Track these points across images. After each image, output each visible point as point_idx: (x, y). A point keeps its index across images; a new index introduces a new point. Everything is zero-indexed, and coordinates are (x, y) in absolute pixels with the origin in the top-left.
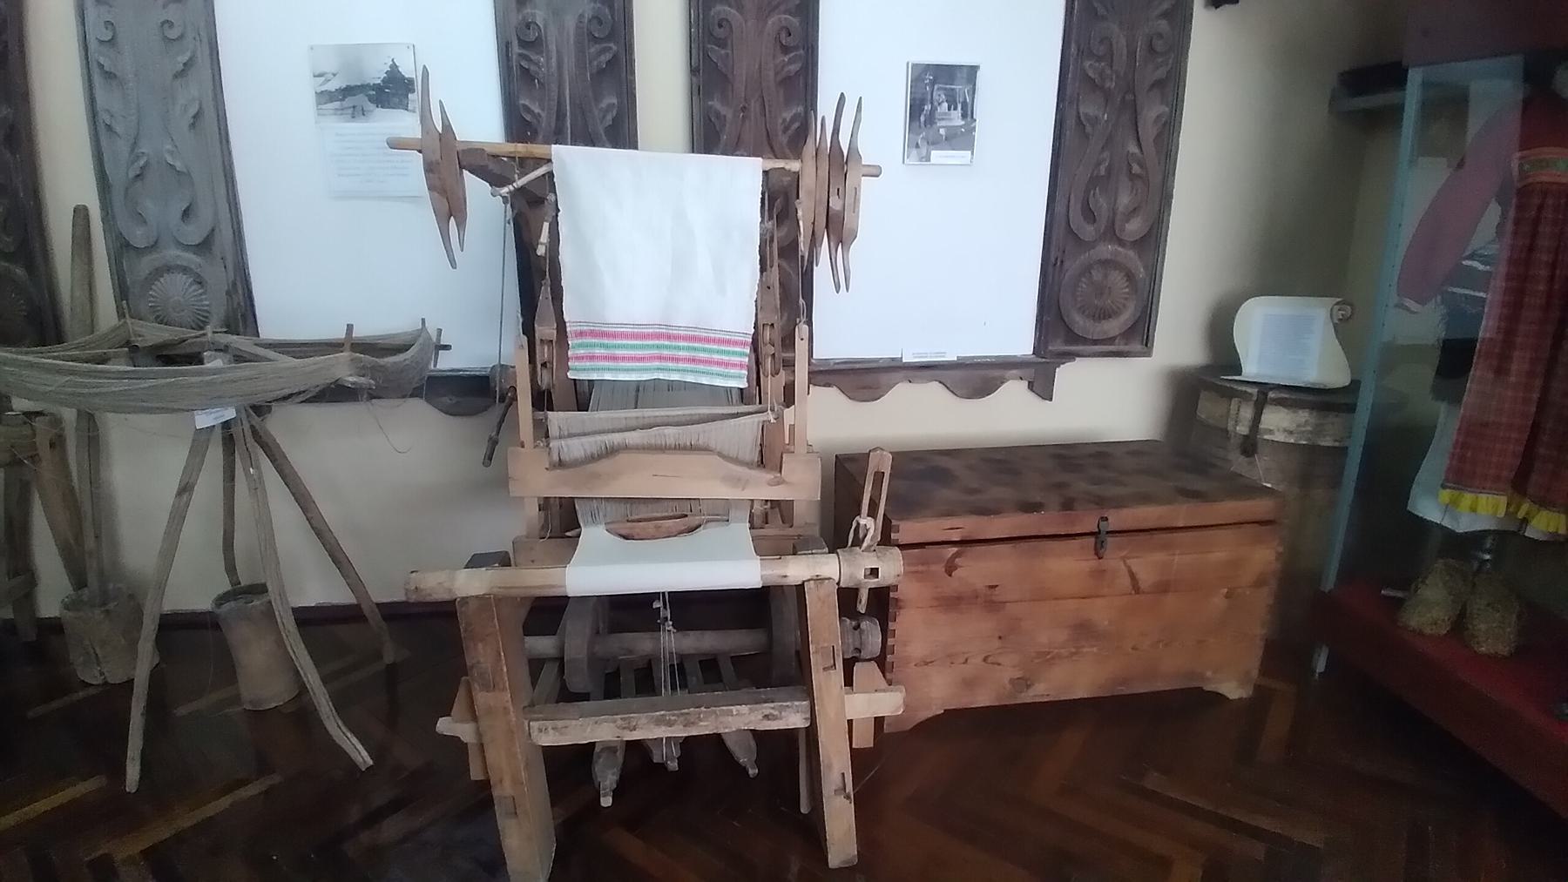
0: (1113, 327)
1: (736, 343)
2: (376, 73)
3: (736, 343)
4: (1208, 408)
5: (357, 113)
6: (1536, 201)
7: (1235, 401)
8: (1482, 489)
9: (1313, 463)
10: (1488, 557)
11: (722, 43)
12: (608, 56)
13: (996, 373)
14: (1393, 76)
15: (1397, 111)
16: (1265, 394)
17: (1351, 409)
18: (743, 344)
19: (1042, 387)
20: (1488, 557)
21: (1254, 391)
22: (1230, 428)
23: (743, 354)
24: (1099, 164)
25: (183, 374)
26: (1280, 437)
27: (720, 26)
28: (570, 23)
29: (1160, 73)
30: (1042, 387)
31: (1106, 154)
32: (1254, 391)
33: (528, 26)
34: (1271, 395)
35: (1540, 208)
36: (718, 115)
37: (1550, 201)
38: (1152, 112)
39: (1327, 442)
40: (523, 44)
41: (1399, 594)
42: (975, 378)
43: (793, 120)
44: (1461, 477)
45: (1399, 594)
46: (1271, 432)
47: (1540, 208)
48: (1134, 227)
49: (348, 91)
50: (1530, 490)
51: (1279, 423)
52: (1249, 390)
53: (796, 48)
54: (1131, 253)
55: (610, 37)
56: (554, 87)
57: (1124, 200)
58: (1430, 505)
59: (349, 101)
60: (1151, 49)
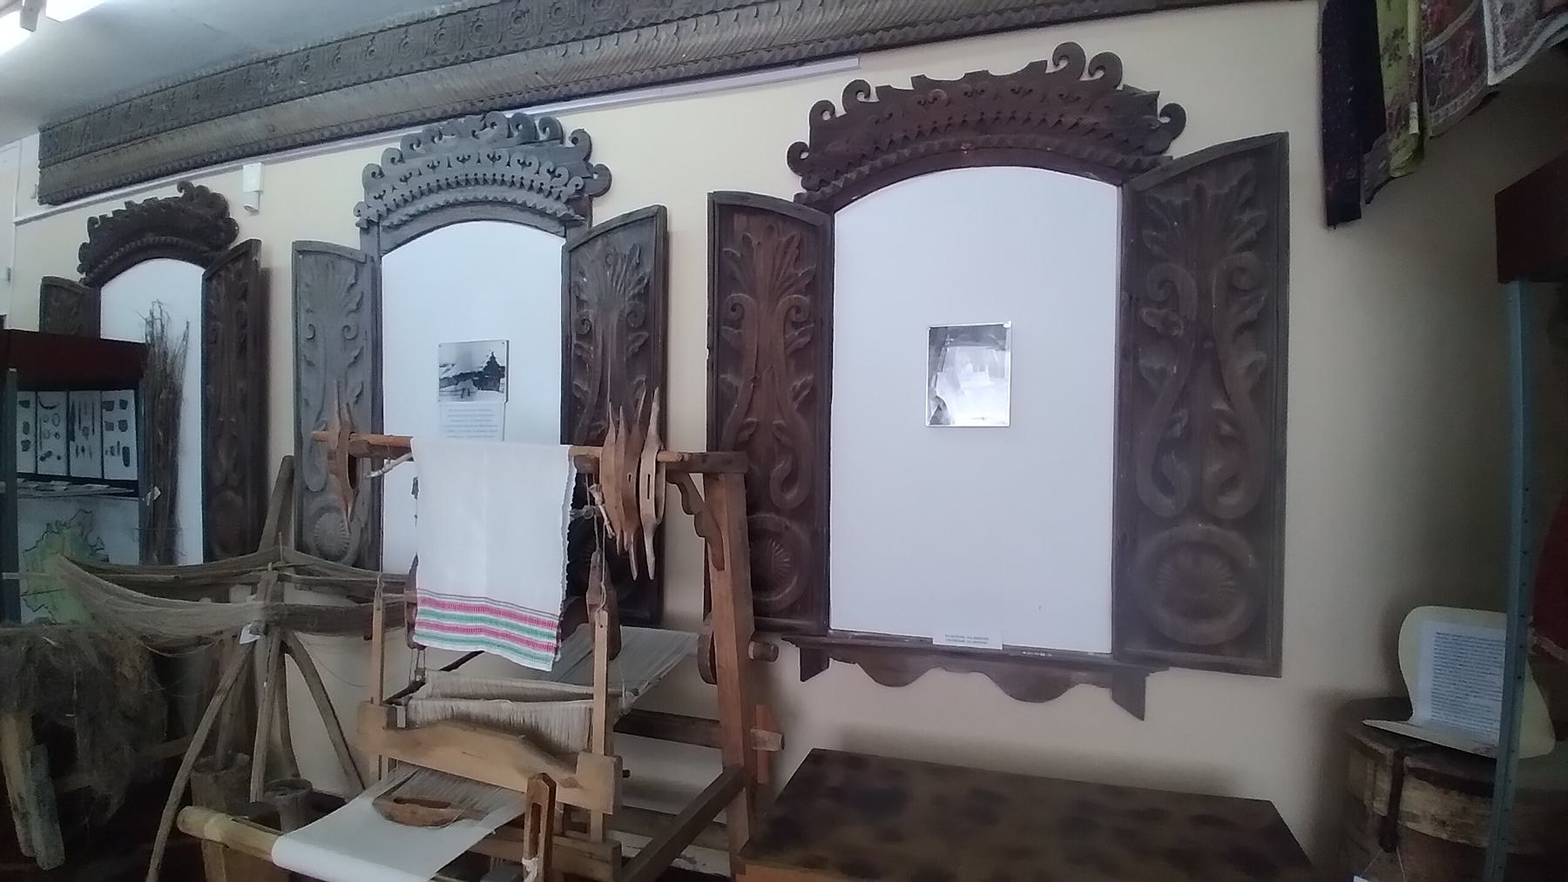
0: (1216, 629)
1: (544, 624)
2: (480, 364)
3: (544, 624)
5: (466, 394)
11: (736, 324)
12: (641, 341)
13: (1058, 673)
18: (550, 625)
19: (1133, 701)
22: (1366, 802)
23: (550, 636)
24: (1172, 424)
25: (179, 606)
26: (1426, 828)
27: (733, 309)
28: (614, 318)
29: (1250, 314)
30: (1133, 701)
31: (1183, 413)
33: (583, 322)
36: (730, 386)
38: (1242, 362)
40: (579, 337)
42: (1035, 675)
43: (803, 387)
46: (1414, 818)
48: (1232, 502)
49: (462, 377)
52: (1381, 749)
53: (807, 322)
54: (1234, 536)
55: (644, 326)
56: (599, 369)
57: (1215, 468)
59: (461, 385)
60: (1232, 290)
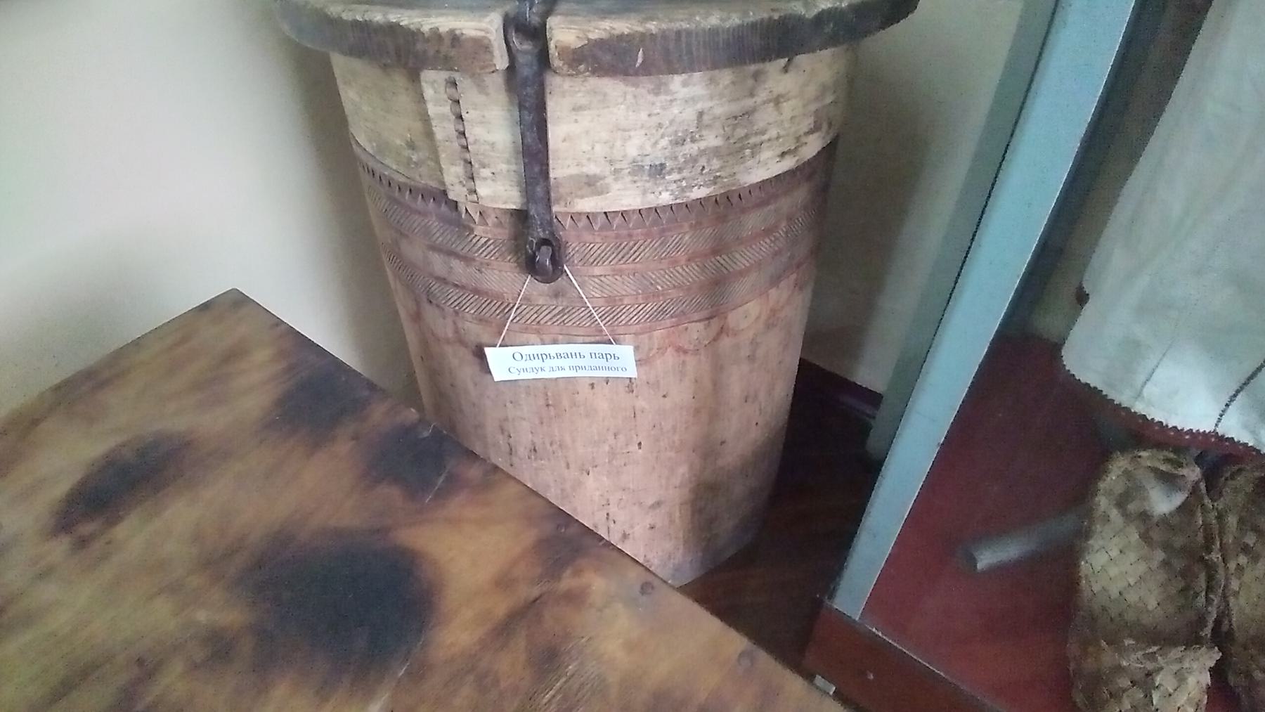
7: (433, 82)
26: (627, 196)
34: (564, 33)
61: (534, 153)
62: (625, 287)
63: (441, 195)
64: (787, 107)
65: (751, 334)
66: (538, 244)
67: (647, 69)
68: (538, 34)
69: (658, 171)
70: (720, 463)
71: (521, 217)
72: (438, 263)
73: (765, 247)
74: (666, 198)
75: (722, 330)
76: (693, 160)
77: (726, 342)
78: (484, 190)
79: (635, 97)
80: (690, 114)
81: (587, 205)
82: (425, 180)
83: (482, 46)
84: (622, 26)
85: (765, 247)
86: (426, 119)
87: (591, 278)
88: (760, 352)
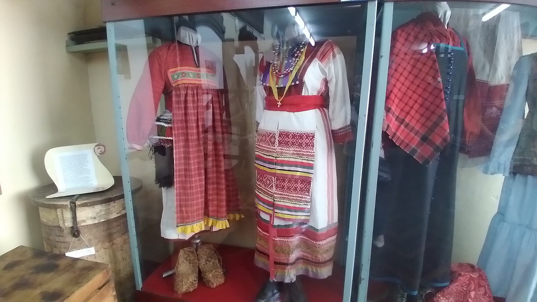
4: (46, 216)
6: (183, 92)
7: (59, 211)
8: (193, 222)
9: (111, 229)
10: (198, 241)
14: (100, 34)
15: (105, 51)
16: (74, 201)
17: (122, 196)
20: (198, 241)
21: (67, 203)
26: (90, 222)
32: (67, 203)
34: (78, 203)
35: (186, 95)
37: (190, 92)
39: (114, 216)
41: (170, 273)
44: (183, 219)
45: (170, 273)
47: (186, 95)
50: (210, 214)
51: (87, 216)
52: (65, 203)
58: (171, 232)
61: (74, 218)
62: (91, 237)
63: (59, 227)
64: (116, 207)
65: (120, 245)
66: (75, 232)
67: (90, 206)
68: (75, 203)
69: (95, 218)
70: (121, 276)
71: (72, 227)
72: (57, 239)
73: (119, 228)
74: (97, 222)
75: (113, 244)
76: (100, 216)
77: (114, 246)
78: (66, 224)
79: (429, 84)
80: (99, 210)
81: (83, 224)
82: (56, 224)
83: (67, 205)
84: (86, 201)
85: (314, 267)
86: (57, 216)
87: (85, 237)
88: (124, 249)
